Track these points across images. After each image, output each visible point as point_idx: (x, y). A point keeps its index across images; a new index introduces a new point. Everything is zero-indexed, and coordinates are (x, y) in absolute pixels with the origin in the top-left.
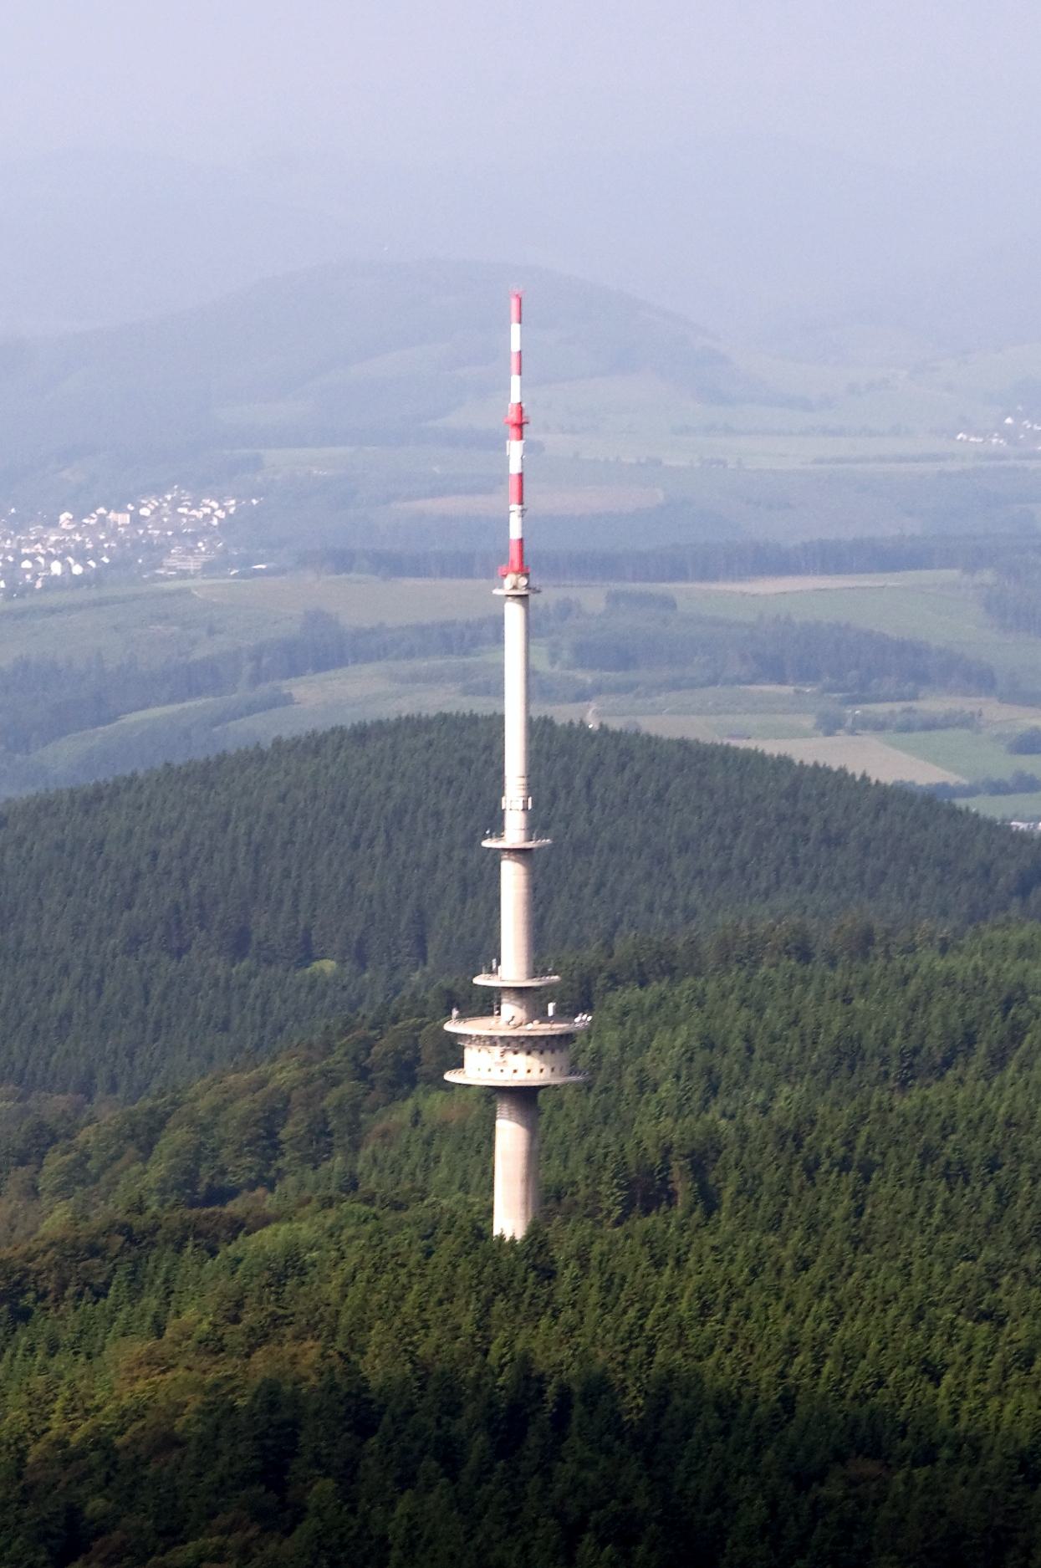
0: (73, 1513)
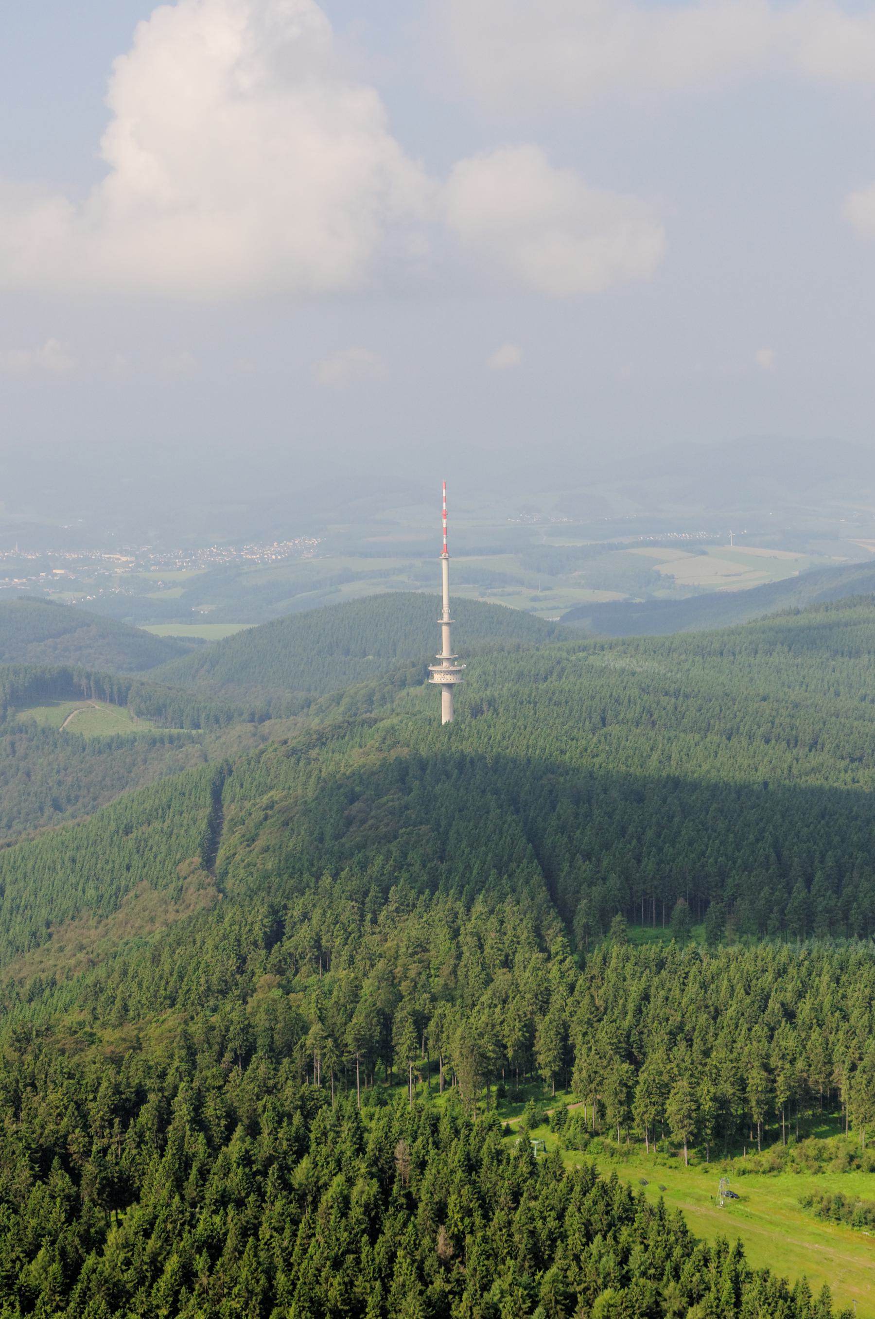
0: (353, 790)
